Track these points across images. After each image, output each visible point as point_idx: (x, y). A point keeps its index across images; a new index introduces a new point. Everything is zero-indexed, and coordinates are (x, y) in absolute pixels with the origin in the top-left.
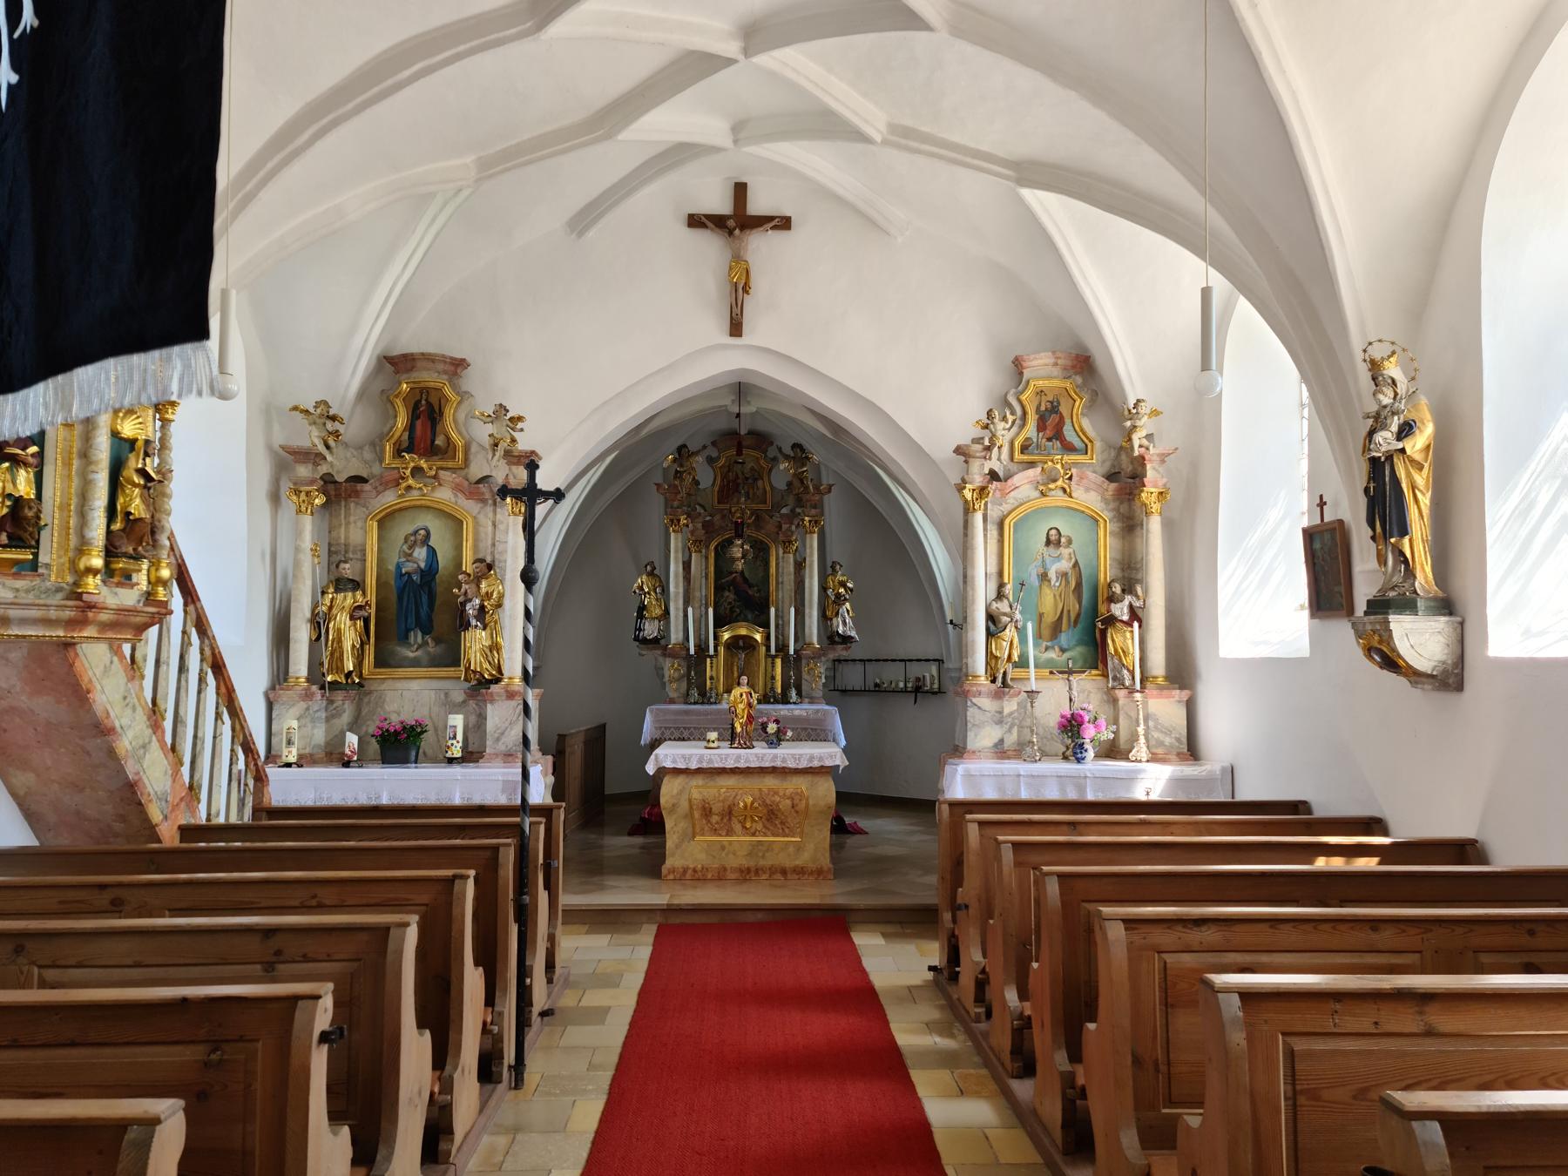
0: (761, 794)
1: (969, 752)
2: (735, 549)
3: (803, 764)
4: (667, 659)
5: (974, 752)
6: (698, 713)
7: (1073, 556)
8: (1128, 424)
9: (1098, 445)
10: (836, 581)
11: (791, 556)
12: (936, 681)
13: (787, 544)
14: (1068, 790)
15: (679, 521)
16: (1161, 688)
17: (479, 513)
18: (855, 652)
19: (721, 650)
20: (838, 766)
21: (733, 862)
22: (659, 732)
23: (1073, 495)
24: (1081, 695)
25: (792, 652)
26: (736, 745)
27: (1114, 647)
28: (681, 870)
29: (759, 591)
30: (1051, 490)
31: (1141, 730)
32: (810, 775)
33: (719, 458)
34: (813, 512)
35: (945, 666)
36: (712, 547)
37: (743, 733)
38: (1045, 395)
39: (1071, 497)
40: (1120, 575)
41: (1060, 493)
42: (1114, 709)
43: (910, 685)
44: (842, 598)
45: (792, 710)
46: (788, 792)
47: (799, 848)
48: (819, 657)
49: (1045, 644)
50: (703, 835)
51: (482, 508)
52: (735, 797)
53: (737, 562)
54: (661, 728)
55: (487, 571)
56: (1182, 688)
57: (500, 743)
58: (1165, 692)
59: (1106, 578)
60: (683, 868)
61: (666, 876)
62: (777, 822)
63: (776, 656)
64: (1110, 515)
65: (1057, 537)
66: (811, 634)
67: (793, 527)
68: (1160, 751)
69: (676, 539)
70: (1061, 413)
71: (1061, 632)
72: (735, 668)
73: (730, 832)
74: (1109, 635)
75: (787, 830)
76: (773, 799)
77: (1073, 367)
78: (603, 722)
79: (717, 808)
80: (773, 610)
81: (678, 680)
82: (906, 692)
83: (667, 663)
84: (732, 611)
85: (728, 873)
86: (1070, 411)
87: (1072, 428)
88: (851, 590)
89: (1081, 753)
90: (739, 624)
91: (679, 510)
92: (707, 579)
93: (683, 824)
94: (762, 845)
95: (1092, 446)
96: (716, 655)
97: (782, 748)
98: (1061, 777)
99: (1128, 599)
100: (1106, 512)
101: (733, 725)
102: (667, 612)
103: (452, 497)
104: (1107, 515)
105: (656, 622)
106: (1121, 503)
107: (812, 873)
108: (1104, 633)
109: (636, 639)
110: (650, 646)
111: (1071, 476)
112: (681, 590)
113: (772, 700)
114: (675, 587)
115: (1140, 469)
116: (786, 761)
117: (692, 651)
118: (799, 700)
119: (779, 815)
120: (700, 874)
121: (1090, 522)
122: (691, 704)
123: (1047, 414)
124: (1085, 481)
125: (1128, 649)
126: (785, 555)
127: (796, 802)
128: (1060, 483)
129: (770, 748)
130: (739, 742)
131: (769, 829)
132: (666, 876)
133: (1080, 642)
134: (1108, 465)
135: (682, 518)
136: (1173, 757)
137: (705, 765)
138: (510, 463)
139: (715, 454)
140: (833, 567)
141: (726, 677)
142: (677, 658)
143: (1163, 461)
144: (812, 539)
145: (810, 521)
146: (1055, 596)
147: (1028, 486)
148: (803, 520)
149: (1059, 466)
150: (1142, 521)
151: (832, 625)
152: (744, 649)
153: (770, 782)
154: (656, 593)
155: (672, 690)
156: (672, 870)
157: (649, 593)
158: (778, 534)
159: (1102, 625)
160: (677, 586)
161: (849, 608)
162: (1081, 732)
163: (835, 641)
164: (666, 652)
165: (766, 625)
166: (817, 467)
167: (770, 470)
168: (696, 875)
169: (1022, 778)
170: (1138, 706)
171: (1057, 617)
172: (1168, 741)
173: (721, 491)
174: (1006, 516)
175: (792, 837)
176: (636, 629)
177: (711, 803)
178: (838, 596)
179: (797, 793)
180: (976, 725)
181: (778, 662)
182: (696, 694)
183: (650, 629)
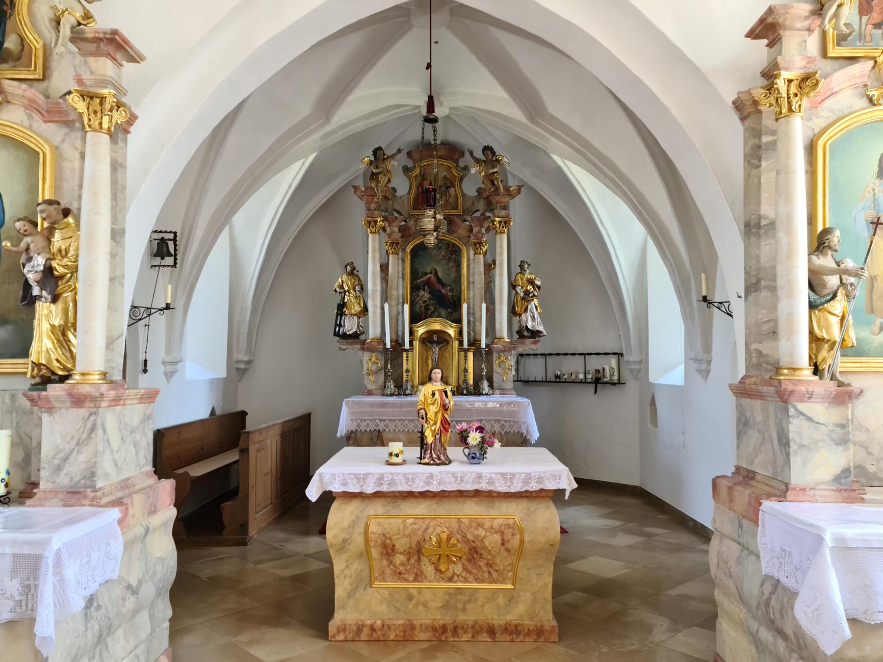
0: (459, 526)
1: (794, 489)
2: (426, 220)
3: (517, 487)
4: (365, 353)
6: (393, 405)
11: (482, 256)
12: (616, 373)
13: (478, 245)
15: (376, 222)
17: (63, 141)
18: (540, 347)
19: (416, 344)
20: (564, 490)
21: (424, 617)
22: (355, 424)
25: (483, 345)
26: (426, 460)
28: (355, 628)
29: (451, 290)
32: (525, 500)
33: (414, 167)
34: (503, 213)
35: (626, 358)
36: (408, 250)
37: (435, 444)
43: (589, 377)
44: (531, 295)
45: (485, 402)
46: (497, 523)
47: (511, 598)
50: (384, 580)
51: (66, 134)
52: (425, 531)
53: (429, 236)
54: (356, 420)
55: (61, 216)
57: (63, 473)
60: (356, 624)
61: (334, 636)
62: (481, 564)
63: (468, 350)
66: (501, 328)
67: (484, 230)
69: (373, 240)
72: (430, 361)
73: (419, 576)
75: (495, 575)
76: (476, 532)
78: (310, 411)
79: (401, 544)
80: (465, 306)
81: (377, 372)
82: (586, 382)
83: (366, 356)
84: (427, 308)
85: (416, 632)
88: (539, 288)
90: (433, 319)
91: (376, 212)
92: (403, 279)
93: (357, 566)
94: (461, 593)
96: (412, 349)
97: (487, 464)
101: (422, 433)
102: (365, 310)
103: (25, 118)
105: (356, 318)
107: (529, 633)
109: (336, 334)
110: (350, 341)
112: (378, 288)
113: (465, 392)
114: (373, 284)
116: (494, 483)
117: (388, 346)
118: (491, 392)
119: (485, 554)
120: (379, 633)
122: (387, 395)
126: (476, 256)
127: (507, 536)
129: (471, 463)
130: (431, 456)
131: (471, 573)
132: (334, 636)
135: (379, 219)
137: (385, 488)
138: (84, 54)
139: (410, 164)
140: (521, 266)
141: (421, 370)
142: (374, 352)
144: (501, 239)
145: (500, 222)
148: (493, 221)
152: (438, 343)
153: (472, 509)
154: (355, 291)
155: (371, 382)
156: (343, 629)
157: (348, 292)
158: (469, 237)
160: (374, 284)
163: (524, 336)
164: (365, 347)
165: (459, 321)
166: (504, 172)
167: (461, 179)
168: (375, 635)
173: (417, 198)
175: (501, 583)
176: (336, 325)
177: (394, 538)
178: (527, 293)
179: (509, 526)
181: (470, 355)
182: (392, 387)
183: (350, 325)
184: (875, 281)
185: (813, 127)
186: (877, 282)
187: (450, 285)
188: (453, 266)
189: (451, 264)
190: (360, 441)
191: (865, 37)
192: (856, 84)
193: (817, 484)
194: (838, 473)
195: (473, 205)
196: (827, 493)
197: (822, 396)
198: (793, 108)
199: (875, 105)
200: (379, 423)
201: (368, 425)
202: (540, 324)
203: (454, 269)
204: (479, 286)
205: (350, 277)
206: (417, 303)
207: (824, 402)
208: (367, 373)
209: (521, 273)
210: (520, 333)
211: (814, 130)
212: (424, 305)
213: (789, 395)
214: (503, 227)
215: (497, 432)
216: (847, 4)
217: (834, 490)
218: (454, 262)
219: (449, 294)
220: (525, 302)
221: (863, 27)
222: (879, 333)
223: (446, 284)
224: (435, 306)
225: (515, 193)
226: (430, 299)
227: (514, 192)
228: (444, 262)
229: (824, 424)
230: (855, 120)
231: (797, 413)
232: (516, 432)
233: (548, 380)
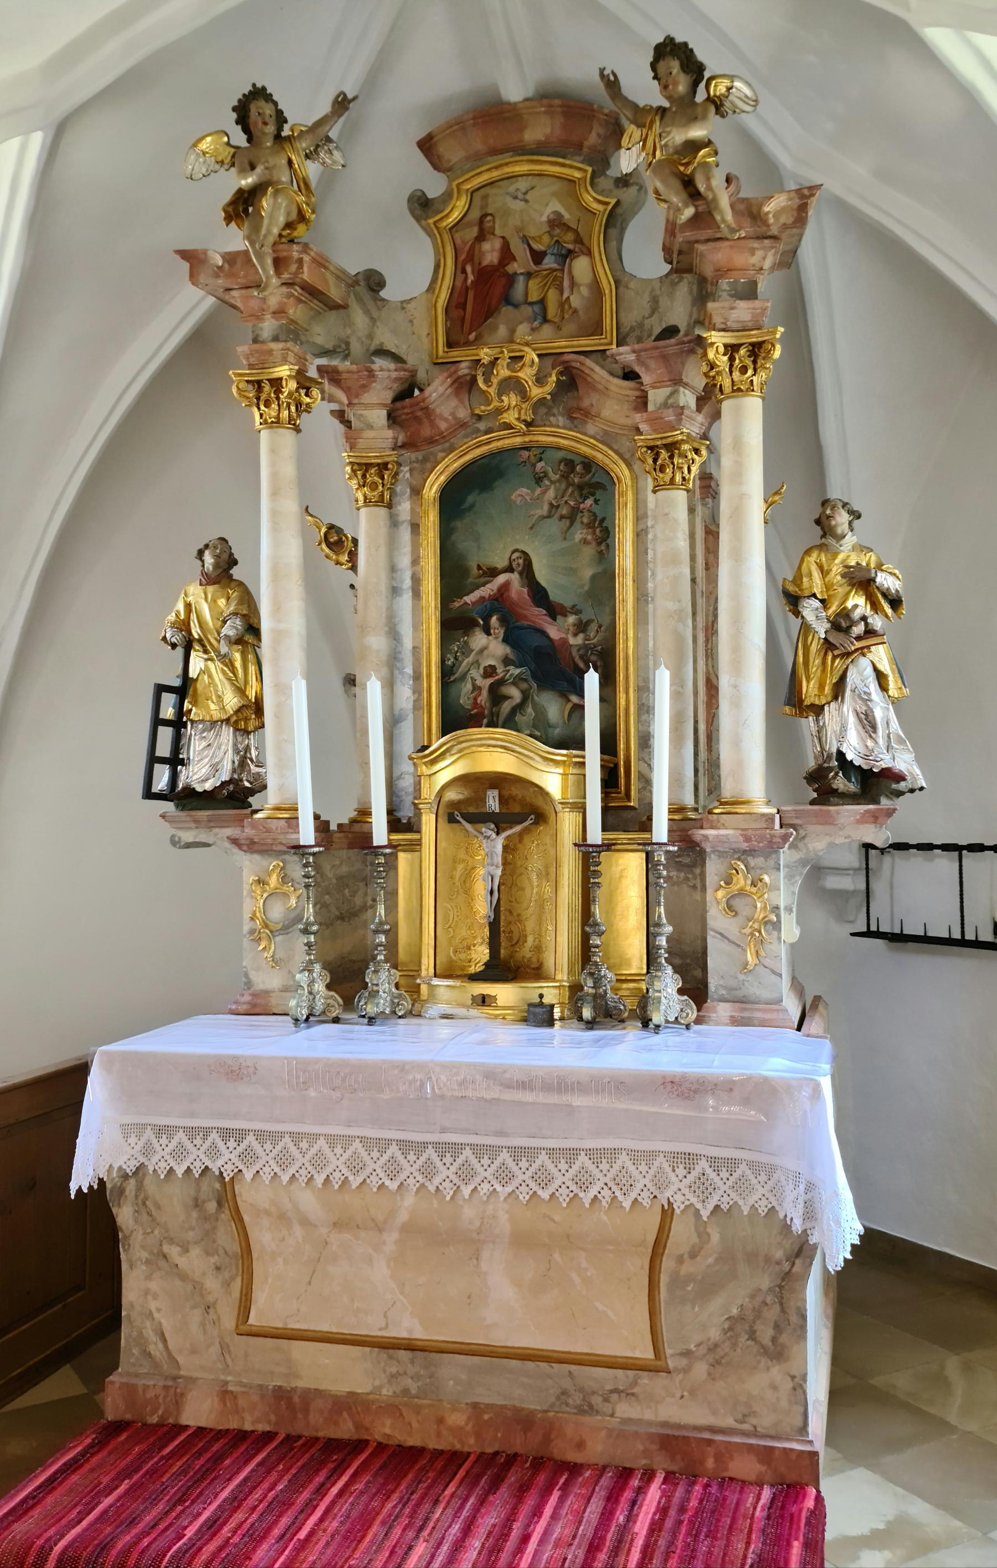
10: (836, 569)
13: (664, 454)
29: (581, 627)
33: (447, 196)
34: (743, 311)
44: (859, 629)
48: (772, 848)
54: (143, 1127)
84: (496, 696)
88: (895, 603)
92: (416, 593)
105: (227, 734)
110: (203, 814)
139: (434, 185)
145: (731, 349)
152: (500, 822)
163: (835, 792)
173: (456, 304)
178: (842, 623)
182: (320, 987)
187: (575, 611)
188: (585, 542)
189: (579, 534)
190: (158, 1207)
195: (654, 309)
200: (220, 1144)
201: (179, 1153)
202: (901, 741)
203: (589, 552)
204: (671, 606)
205: (210, 589)
206: (463, 678)
208: (252, 932)
209: (822, 547)
210: (818, 777)
212: (490, 681)
214: (744, 370)
215: (678, 1207)
218: (590, 526)
219: (572, 641)
220: (834, 657)
223: (562, 607)
224: (524, 686)
225: (785, 227)
226: (506, 661)
227: (783, 219)
228: (554, 526)
232: (763, 1211)
233: (970, 936)
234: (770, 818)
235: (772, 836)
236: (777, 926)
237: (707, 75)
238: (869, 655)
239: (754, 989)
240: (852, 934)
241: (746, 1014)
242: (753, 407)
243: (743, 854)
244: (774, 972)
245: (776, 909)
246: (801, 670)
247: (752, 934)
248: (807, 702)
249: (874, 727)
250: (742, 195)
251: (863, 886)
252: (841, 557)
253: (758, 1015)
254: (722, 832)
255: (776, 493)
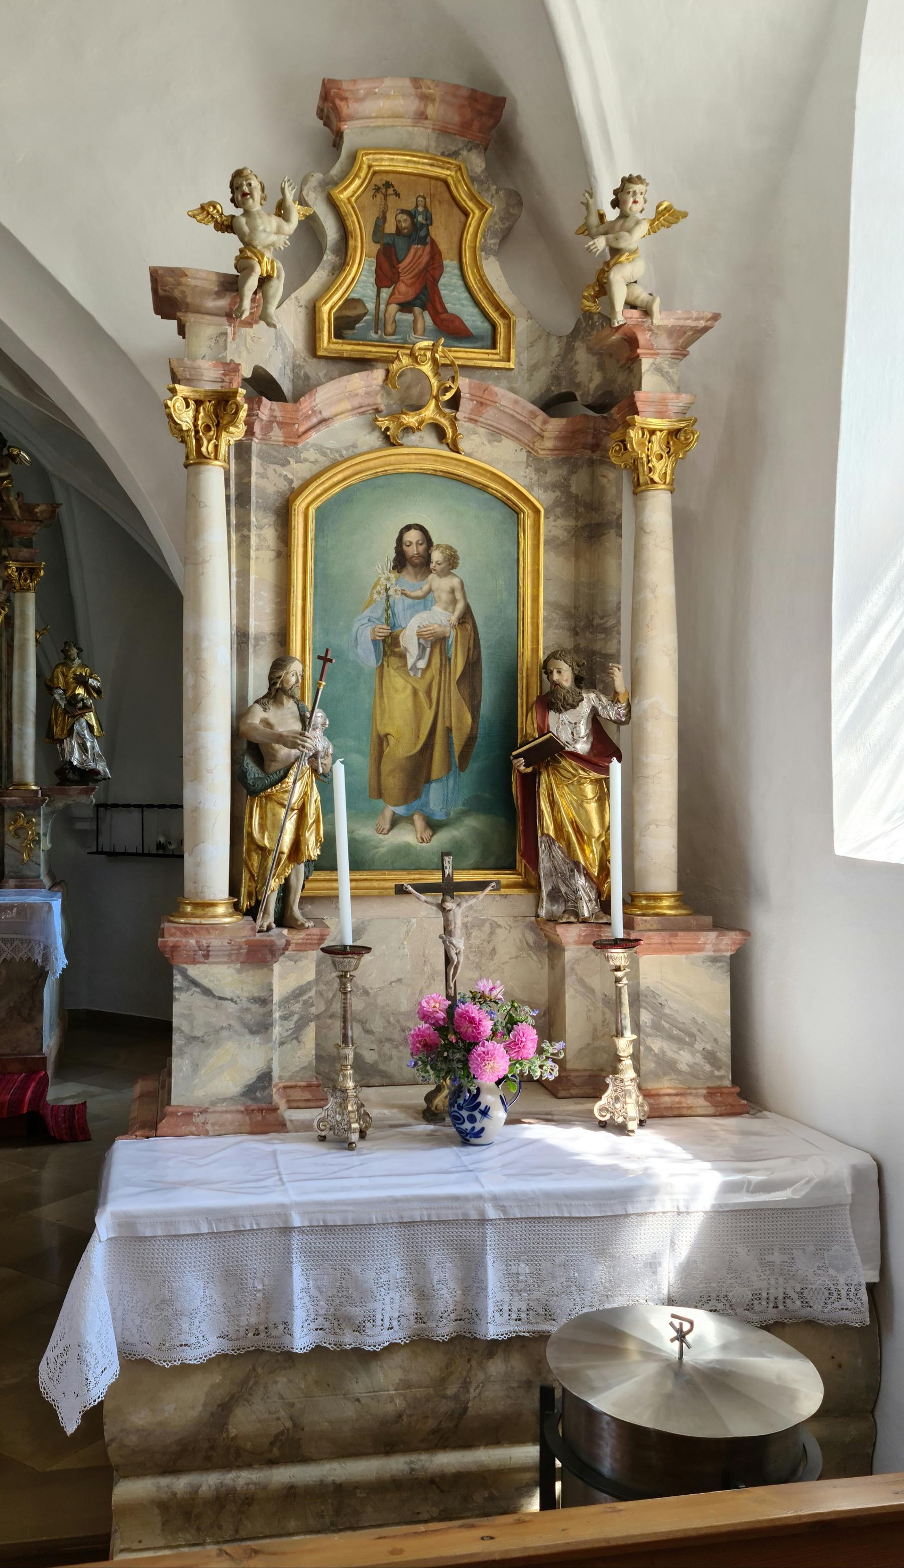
1: (174, 1114)
5: (189, 1114)
7: (459, 595)
8: (601, 243)
9: (521, 326)
10: (71, 675)
14: (432, 1263)
16: (670, 926)
23: (462, 445)
24: (475, 933)
27: (555, 821)
30: (408, 429)
31: (624, 1045)
34: (25, 553)
38: (397, 194)
39: (458, 452)
40: (568, 644)
41: (430, 439)
42: (552, 967)
44: (80, 705)
48: (37, 805)
49: (389, 810)
56: (720, 926)
58: (683, 937)
59: (535, 651)
64: (549, 497)
65: (421, 548)
66: (22, 767)
68: (665, 1085)
70: (433, 242)
71: (428, 781)
74: (543, 790)
77: (465, 128)
86: (456, 239)
87: (460, 283)
88: (98, 691)
89: (472, 1119)
95: (509, 327)
98: (412, 1224)
99: (590, 700)
100: (538, 491)
104: (539, 498)
106: (573, 469)
108: (530, 785)
111: (458, 393)
115: (621, 377)
121: (498, 513)
123: (400, 243)
124: (489, 414)
125: (589, 824)
128: (429, 412)
133: (474, 806)
134: (543, 376)
136: (699, 1103)
143: (681, 353)
144: (23, 601)
146: (415, 692)
147: (351, 419)
149: (427, 368)
150: (620, 517)
151: (63, 750)
159: (527, 766)
161: (94, 722)
162: (472, 1065)
169: (296, 1240)
170: (618, 980)
171: (419, 747)
172: (685, 1059)
174: (295, 493)
178: (73, 700)
180: (195, 1038)
184: (385, 743)
185: (290, 476)
186: (388, 745)
191: (385, 325)
192: (362, 407)
193: (213, 1103)
194: (251, 1082)
196: (229, 1117)
197: (227, 953)
198: (204, 449)
199: (393, 445)
207: (232, 962)
209: (64, 664)
211: (291, 482)
213: (172, 952)
214: (26, 580)
216: (279, 277)
217: (242, 1112)
221: (382, 307)
222: (389, 831)
227: (44, 515)
229: (232, 1000)
230: (363, 466)
231: (186, 983)
232: (25, 959)
233: (146, 851)
234: (36, 791)
235: (37, 800)
236: (38, 842)
237: (8, 444)
238: (85, 717)
239: (27, 872)
240: (89, 853)
241: (22, 884)
242: (31, 597)
243: (23, 809)
244: (36, 864)
245: (38, 834)
246: (53, 721)
247: (27, 846)
248: (56, 737)
249: (87, 751)
250: (24, 502)
251: (95, 828)
252: (73, 669)
253: (29, 883)
254: (13, 798)
255: (44, 629)
